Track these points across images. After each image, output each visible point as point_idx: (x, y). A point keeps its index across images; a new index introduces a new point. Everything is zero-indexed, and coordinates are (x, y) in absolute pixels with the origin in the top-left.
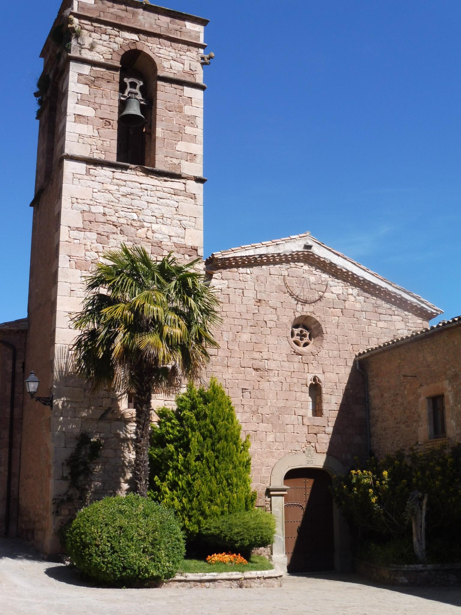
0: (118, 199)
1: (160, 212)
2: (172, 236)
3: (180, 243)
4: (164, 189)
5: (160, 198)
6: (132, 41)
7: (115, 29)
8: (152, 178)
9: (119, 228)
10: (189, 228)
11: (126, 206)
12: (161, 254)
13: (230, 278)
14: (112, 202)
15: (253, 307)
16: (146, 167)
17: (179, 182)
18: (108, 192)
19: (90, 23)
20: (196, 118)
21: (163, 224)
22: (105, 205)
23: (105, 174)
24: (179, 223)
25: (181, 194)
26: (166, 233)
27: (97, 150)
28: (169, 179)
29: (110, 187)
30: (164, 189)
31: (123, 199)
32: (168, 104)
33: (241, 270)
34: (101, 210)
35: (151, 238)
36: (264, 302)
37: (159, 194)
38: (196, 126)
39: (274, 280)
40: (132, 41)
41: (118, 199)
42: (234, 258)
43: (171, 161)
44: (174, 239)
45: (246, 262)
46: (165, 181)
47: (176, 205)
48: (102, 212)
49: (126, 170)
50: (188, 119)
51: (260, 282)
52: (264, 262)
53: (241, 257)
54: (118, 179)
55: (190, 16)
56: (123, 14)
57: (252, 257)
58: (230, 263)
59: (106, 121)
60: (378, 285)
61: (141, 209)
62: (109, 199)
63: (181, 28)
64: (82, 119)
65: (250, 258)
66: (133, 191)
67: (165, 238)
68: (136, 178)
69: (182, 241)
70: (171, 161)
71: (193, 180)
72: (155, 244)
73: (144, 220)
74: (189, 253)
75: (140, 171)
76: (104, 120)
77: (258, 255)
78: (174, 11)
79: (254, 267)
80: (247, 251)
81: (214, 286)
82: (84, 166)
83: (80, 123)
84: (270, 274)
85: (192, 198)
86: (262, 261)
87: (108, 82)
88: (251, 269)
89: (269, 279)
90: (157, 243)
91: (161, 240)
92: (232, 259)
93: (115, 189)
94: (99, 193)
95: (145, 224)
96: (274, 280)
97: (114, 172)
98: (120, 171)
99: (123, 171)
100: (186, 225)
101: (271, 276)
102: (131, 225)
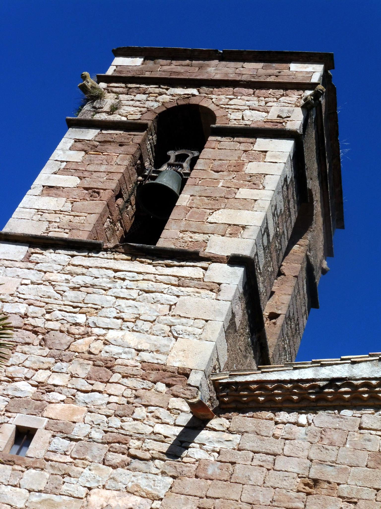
0: (62, 292)
1: (136, 312)
2: (144, 351)
3: (156, 361)
4: (158, 277)
5: (147, 292)
6: (186, 96)
7: (161, 86)
8: (142, 262)
9: (41, 337)
10: (187, 337)
11: (71, 304)
12: (106, 380)
13: (247, 429)
14: (49, 297)
15: (294, 494)
16: (131, 244)
17: (193, 266)
18: (48, 284)
19: (123, 85)
20: (267, 176)
21: (133, 331)
22: (32, 302)
23: (55, 259)
24: (167, 329)
25: (191, 284)
26: (132, 345)
27: (59, 228)
28: (176, 263)
29: (54, 277)
30: (158, 277)
31: (71, 295)
32: (217, 163)
33: (283, 416)
34: (22, 308)
35: (96, 352)
36: (326, 485)
37: (145, 285)
38: (261, 187)
39: (369, 440)
40: (186, 96)
41: (62, 292)
42: (262, 384)
43: (191, 237)
44: (145, 356)
45: (295, 397)
46: (168, 266)
47: (174, 299)
48: (121, 376)
49: (98, 252)
50: (249, 179)
51: (326, 442)
52: (344, 400)
53: (280, 383)
54: (77, 266)
55: (298, 53)
56: (179, 69)
57: (308, 385)
58: (253, 398)
59: (95, 192)
60: (185, 89)
61: (100, 307)
62: (45, 294)
63: (279, 72)
64: (54, 191)
65: (304, 386)
66: (96, 281)
67: (125, 353)
68: (112, 264)
69: (162, 359)
70: (191, 237)
71: (224, 263)
72: (100, 363)
73: (95, 324)
74: (170, 381)
75: (123, 253)
76: (90, 191)
77: (324, 380)
78: (269, 52)
79: (320, 412)
80: (297, 371)
81: (204, 445)
82: (23, 250)
83: (48, 196)
84: (360, 428)
85: (211, 290)
86: (338, 396)
87: (121, 145)
88: (311, 416)
89: (356, 437)
90: (105, 361)
91: (115, 357)
92: (255, 386)
93: (64, 278)
94: (31, 286)
95: (96, 331)
96: (369, 440)
97: (73, 256)
98: (86, 254)
99: (90, 254)
100: (181, 332)
101: (362, 431)
102: (68, 332)
